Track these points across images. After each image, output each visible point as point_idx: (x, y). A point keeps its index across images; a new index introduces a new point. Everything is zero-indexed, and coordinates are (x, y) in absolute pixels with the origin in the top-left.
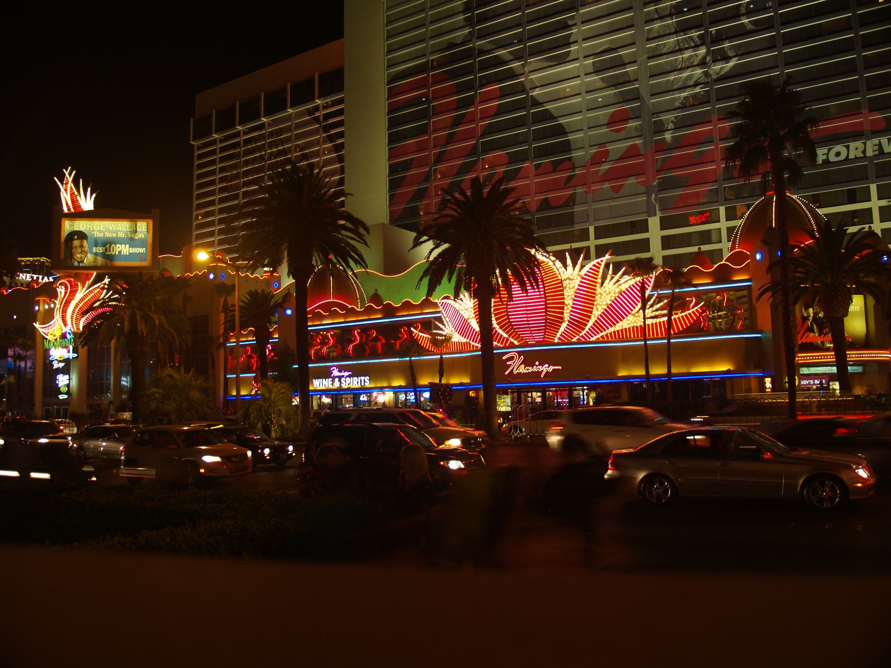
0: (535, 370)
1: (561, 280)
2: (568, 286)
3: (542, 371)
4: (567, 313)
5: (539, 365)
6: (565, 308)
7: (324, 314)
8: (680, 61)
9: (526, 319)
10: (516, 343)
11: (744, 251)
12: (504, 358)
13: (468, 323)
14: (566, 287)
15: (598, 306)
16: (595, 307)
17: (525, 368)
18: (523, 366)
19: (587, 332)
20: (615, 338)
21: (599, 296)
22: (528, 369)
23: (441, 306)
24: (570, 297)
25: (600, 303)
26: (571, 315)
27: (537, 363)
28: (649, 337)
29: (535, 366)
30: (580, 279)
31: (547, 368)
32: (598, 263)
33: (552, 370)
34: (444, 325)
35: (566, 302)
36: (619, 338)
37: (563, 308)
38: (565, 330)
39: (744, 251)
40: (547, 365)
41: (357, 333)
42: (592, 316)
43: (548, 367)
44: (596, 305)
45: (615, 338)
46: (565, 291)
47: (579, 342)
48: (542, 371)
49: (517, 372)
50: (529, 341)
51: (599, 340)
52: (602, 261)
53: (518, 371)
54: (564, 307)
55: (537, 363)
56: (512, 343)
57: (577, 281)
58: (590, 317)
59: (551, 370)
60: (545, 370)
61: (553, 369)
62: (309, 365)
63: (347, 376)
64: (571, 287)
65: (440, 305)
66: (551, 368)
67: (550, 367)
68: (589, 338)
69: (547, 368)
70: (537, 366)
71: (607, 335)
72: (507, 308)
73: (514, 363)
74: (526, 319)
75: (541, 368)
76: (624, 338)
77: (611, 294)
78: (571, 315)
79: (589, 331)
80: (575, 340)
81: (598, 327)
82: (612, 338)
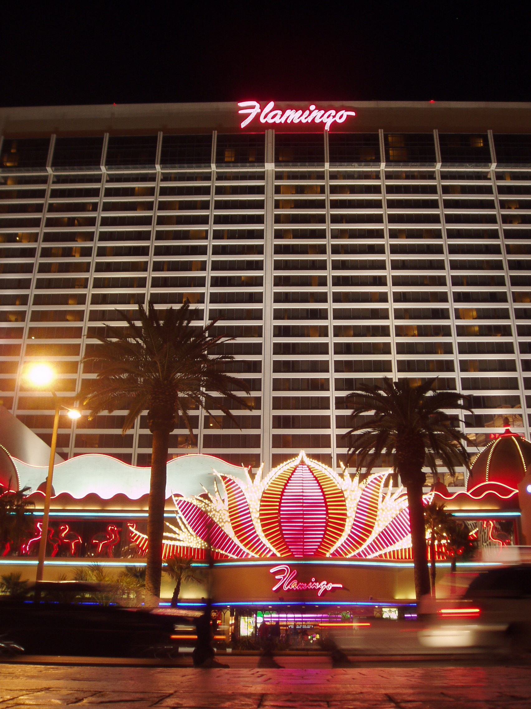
0: (311, 587)
1: (342, 490)
2: (350, 496)
3: (319, 589)
4: (348, 525)
5: (316, 581)
6: (347, 520)
7: (30, 541)
8: (29, 696)
9: (302, 524)
10: (278, 555)
11: (15, 646)
12: (272, 571)
13: (270, 486)
14: (347, 498)
15: (380, 522)
16: (376, 523)
17: (298, 584)
18: (295, 582)
19: (365, 549)
20: (394, 558)
21: (381, 511)
22: (301, 586)
23: (178, 504)
24: (352, 509)
25: (382, 519)
26: (353, 528)
27: (313, 580)
28: (439, 560)
29: (311, 583)
30: (361, 492)
31: (325, 585)
32: (380, 477)
33: (331, 588)
34: (180, 528)
35: (348, 513)
36: (398, 558)
37: (344, 520)
38: (342, 545)
39: (15, 646)
40: (325, 582)
41: (40, 525)
42: (373, 532)
43: (327, 585)
44: (378, 521)
45: (394, 558)
46: (347, 501)
47: (353, 559)
48: (319, 589)
49: (287, 588)
50: (296, 554)
51: (377, 558)
52: (384, 475)
53: (289, 587)
54: (346, 518)
55: (313, 580)
56: (274, 555)
57: (359, 493)
58: (370, 532)
59: (330, 589)
60: (322, 588)
61: (332, 587)
62: (196, 637)
63: (368, 687)
64: (353, 498)
65: (176, 503)
66: (330, 586)
67: (329, 585)
68: (366, 556)
69: (325, 585)
70: (313, 583)
71: (385, 554)
72: (280, 506)
73: (284, 577)
74: (302, 524)
75: (318, 585)
76: (410, 559)
77: (393, 511)
78: (353, 528)
79: (367, 548)
80: (349, 556)
81: (372, 548)
82: (390, 557)
